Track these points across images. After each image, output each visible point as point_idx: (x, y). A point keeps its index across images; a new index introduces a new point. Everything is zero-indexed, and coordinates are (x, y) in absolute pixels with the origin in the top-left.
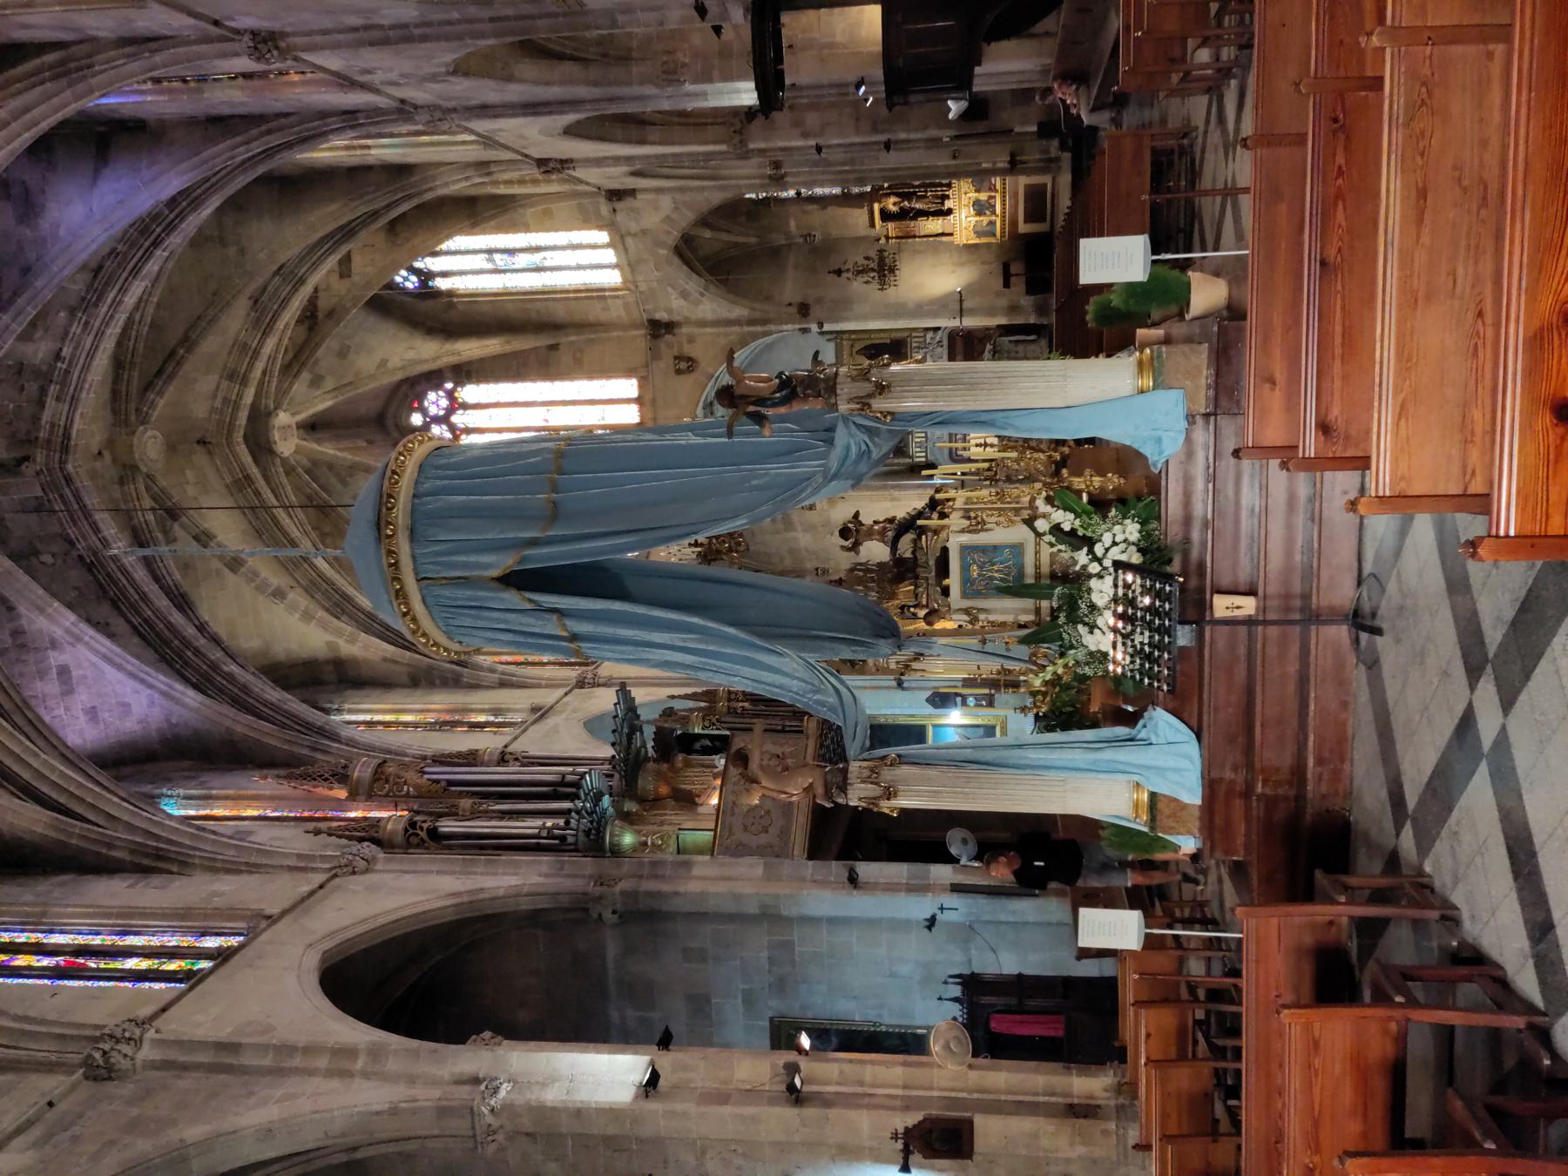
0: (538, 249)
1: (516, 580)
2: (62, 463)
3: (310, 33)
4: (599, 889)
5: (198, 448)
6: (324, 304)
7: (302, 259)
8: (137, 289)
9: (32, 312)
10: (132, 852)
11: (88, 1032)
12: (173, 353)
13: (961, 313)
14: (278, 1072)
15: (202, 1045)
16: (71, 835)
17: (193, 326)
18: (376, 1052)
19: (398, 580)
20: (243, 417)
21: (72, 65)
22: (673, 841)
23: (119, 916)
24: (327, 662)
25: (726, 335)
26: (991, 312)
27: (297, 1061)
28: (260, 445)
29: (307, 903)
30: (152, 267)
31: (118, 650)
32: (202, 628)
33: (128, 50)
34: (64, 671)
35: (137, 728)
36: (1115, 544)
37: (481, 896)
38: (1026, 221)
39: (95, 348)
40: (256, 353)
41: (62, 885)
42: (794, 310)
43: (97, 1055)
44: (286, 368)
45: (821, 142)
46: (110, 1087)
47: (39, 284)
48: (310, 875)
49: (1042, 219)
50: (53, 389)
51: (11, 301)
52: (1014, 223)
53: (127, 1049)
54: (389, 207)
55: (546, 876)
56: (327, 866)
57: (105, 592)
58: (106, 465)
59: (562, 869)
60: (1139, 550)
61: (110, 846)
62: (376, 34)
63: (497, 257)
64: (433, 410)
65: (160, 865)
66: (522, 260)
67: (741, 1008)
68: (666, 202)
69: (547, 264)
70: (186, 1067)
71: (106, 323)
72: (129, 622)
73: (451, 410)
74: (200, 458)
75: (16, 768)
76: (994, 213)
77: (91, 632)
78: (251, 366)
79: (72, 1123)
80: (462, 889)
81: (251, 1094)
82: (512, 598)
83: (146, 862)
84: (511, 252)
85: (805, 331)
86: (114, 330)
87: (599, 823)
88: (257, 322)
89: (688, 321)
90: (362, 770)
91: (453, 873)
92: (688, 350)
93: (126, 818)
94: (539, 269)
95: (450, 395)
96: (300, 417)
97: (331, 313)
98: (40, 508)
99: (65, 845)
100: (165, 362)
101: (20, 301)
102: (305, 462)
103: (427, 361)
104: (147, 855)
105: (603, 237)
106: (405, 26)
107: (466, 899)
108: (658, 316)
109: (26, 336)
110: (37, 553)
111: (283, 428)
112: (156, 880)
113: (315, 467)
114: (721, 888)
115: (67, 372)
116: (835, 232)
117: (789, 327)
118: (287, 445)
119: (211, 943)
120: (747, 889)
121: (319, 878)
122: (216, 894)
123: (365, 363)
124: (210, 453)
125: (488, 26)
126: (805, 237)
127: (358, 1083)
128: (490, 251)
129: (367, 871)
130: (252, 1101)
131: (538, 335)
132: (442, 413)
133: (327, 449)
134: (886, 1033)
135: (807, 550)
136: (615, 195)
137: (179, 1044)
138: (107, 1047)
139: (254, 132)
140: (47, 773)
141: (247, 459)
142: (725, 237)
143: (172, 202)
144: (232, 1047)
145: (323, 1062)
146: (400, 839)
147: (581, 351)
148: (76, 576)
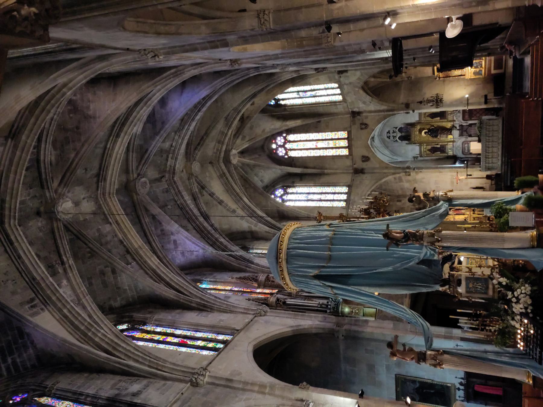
0: (314, 90)
1: (317, 277)
2: (173, 177)
3: (247, 59)
4: (338, 328)
5: (209, 165)
6: (245, 116)
7: (239, 105)
8: (194, 124)
9: (165, 135)
10: (197, 304)
11: (190, 371)
12: (202, 138)
13: (468, 104)
14: (244, 390)
15: (221, 379)
16: (181, 299)
17: (207, 130)
18: (272, 387)
19: (283, 275)
20: (222, 155)
21: (179, 73)
22: (362, 311)
23: (195, 325)
24: (248, 232)
25: (379, 115)
26: (480, 104)
27: (249, 387)
28: (227, 161)
29: (248, 326)
30: (198, 117)
31: (190, 235)
32: (212, 226)
33: (194, 67)
34: (175, 241)
35: (195, 258)
36: (521, 293)
37: (300, 328)
38: (494, 69)
39: (182, 143)
40: (226, 134)
41: (179, 313)
42: (404, 106)
43: (194, 379)
44: (235, 135)
45: (415, 56)
46: (197, 389)
47: (167, 126)
48: (248, 315)
49: (501, 68)
50: (170, 155)
51: (159, 132)
52: (489, 70)
53: (202, 378)
54: (266, 87)
55: (321, 321)
56: (253, 313)
57: (186, 216)
58: (184, 175)
59: (325, 319)
60: (531, 298)
61: (191, 302)
62: (268, 57)
63: (300, 93)
64: (279, 143)
65: (205, 309)
66: (309, 94)
67: (385, 370)
68: (358, 73)
69: (317, 94)
70: (218, 385)
71: (185, 136)
72: (192, 225)
73: (285, 143)
74: (210, 168)
75: (165, 277)
76: (481, 67)
77: (183, 230)
78: (225, 138)
79: (189, 401)
80: (294, 325)
81: (237, 396)
82: (317, 282)
83: (201, 308)
84: (305, 91)
85: (407, 113)
86: (187, 137)
87: (337, 305)
88: (227, 124)
89: (365, 111)
90: (262, 277)
91: (291, 318)
92: (365, 121)
93: (195, 293)
94: (314, 96)
95: (285, 138)
96: (239, 151)
97: (248, 117)
98: (167, 191)
99: (179, 301)
100: (200, 140)
101: (162, 132)
102: (240, 164)
103: (278, 129)
104: (201, 306)
105: (336, 85)
106: (277, 55)
107: (295, 328)
108: (355, 110)
109: (164, 141)
110: (167, 206)
111: (235, 155)
112: (204, 314)
113: (244, 165)
114: (378, 331)
115: (174, 150)
116: (419, 76)
117: (402, 112)
118: (235, 160)
119: (221, 337)
120: (386, 332)
121: (251, 317)
122: (221, 320)
123: (258, 131)
124: (213, 166)
125: (303, 53)
126: (408, 78)
127: (267, 396)
128: (298, 92)
129: (265, 315)
130: (237, 399)
131: (313, 118)
132: (282, 144)
133: (246, 160)
134: (437, 384)
135: (408, 189)
136: (340, 72)
137: (216, 378)
138: (196, 377)
139: (227, 76)
140: (173, 279)
141: (223, 167)
142: (379, 80)
143: (204, 99)
144: (230, 380)
145: (256, 388)
146: (274, 304)
147: (328, 123)
148: (178, 212)
